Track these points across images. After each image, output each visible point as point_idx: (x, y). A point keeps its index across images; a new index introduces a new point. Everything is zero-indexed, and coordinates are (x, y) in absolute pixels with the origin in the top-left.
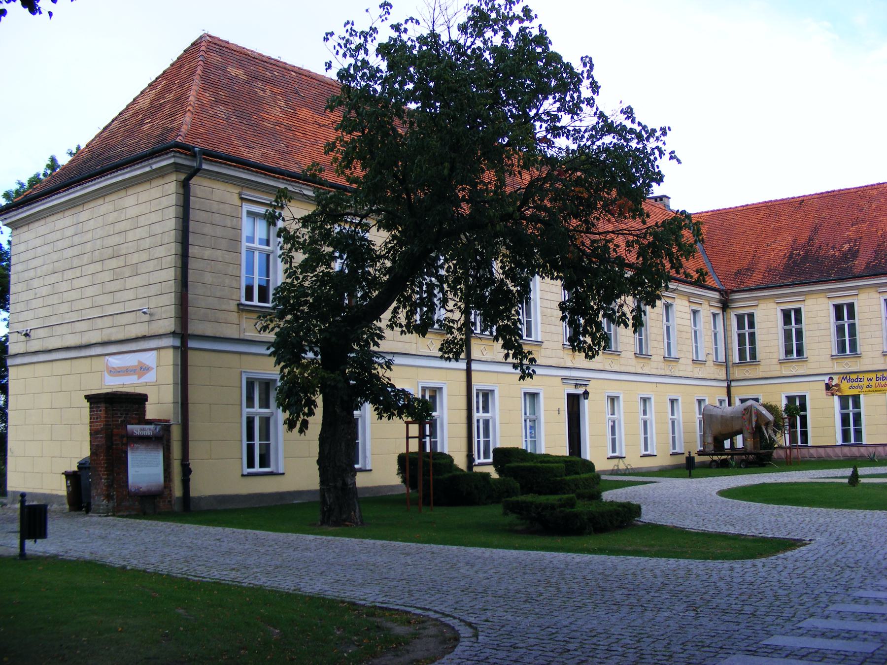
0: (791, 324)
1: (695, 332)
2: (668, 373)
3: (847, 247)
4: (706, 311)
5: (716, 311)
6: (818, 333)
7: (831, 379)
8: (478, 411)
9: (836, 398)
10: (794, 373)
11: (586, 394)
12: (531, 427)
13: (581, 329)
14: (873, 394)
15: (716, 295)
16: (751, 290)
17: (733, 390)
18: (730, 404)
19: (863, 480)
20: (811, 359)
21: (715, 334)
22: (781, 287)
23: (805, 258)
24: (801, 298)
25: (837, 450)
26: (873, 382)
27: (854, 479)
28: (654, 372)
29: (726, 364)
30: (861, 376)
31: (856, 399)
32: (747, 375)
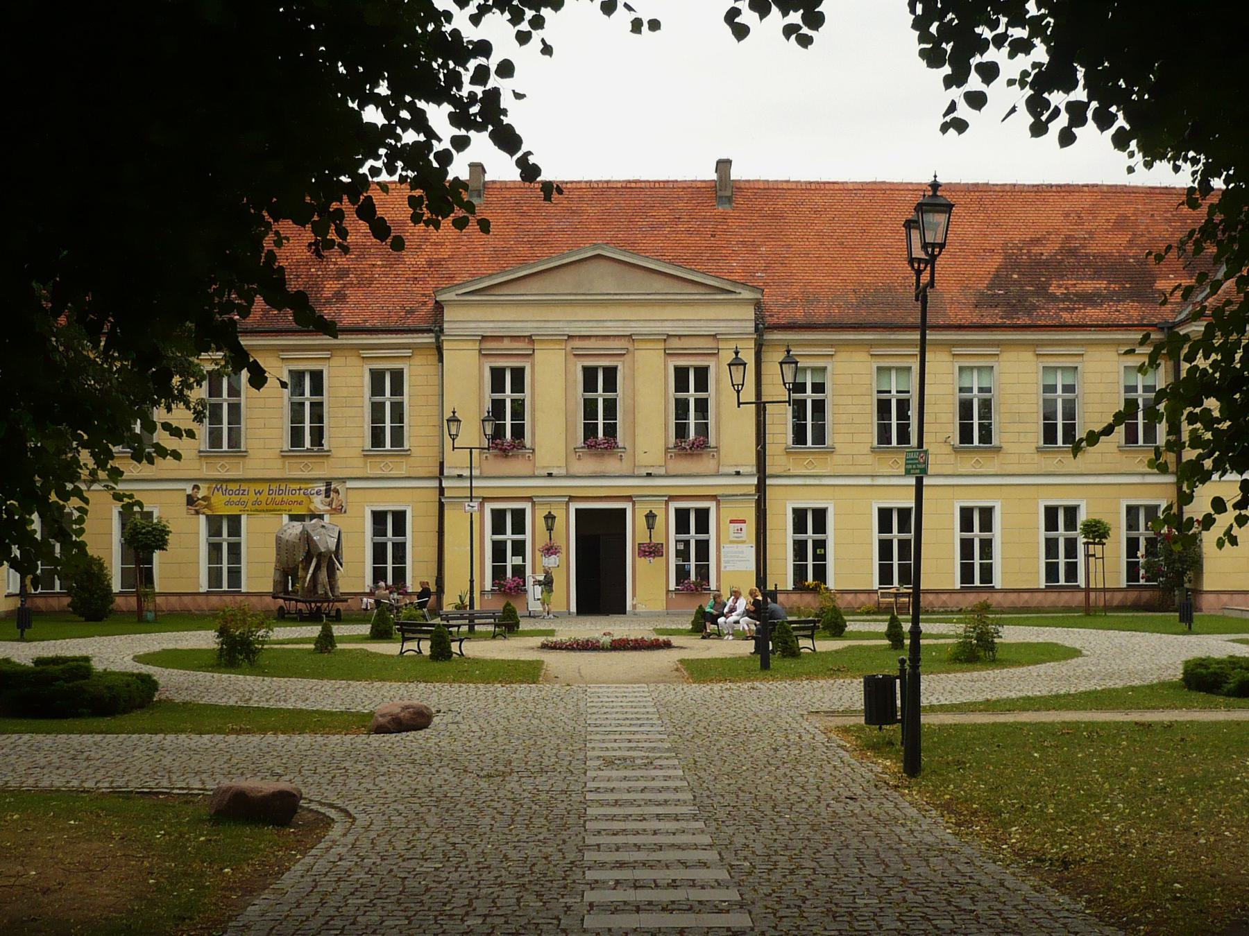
7: (196, 487)
9: (202, 518)
14: (262, 515)
16: (960, 327)
18: (744, 522)
19: (339, 646)
24: (408, 353)
25: (1040, 596)
26: (263, 498)
30: (244, 486)
31: (235, 522)
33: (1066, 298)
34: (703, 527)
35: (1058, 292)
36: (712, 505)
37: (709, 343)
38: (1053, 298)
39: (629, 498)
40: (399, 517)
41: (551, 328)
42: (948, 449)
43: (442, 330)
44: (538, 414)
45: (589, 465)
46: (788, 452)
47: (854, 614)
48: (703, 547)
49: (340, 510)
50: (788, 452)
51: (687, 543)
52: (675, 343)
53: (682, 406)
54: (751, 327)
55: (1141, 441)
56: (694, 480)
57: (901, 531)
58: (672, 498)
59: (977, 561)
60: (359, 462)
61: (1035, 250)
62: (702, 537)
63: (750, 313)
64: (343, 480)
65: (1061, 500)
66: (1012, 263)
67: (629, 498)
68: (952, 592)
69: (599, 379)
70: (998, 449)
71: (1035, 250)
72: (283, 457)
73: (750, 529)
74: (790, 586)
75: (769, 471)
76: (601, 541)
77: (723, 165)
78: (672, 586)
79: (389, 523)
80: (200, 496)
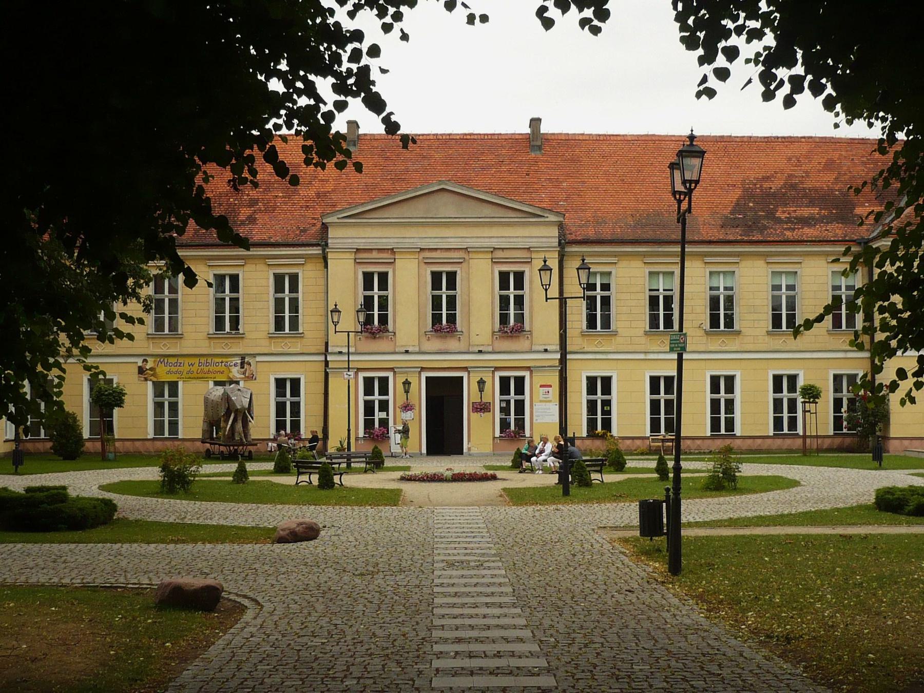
9: (150, 384)
14: (194, 381)
16: (710, 242)
19: (251, 478)
24: (302, 261)
26: (194, 369)
27: (241, 475)
30: (181, 360)
31: (174, 387)
32: (286, 350)
33: (789, 220)
34: (520, 390)
35: (783, 216)
36: (527, 374)
37: (525, 254)
38: (779, 221)
39: (465, 369)
40: (295, 383)
41: (408, 243)
42: (701, 333)
43: (327, 245)
44: (398, 307)
46: (583, 334)
47: (632, 454)
48: (520, 405)
49: (252, 377)
50: (583, 334)
51: (508, 402)
52: (499, 254)
53: (504, 301)
54: (555, 242)
55: (844, 327)
56: (513, 356)
57: (666, 393)
58: (497, 369)
59: (723, 416)
60: (266, 342)
61: (766, 185)
62: (519, 397)
63: (555, 232)
64: (254, 355)
65: (785, 370)
66: (748, 194)
67: (465, 369)
68: (704, 438)
69: (443, 280)
70: (739, 333)
71: (766, 185)
72: (210, 338)
73: (555, 391)
74: (585, 434)
75: (569, 349)
76: (444, 400)
78: (497, 434)
79: (288, 387)
80: (148, 367)
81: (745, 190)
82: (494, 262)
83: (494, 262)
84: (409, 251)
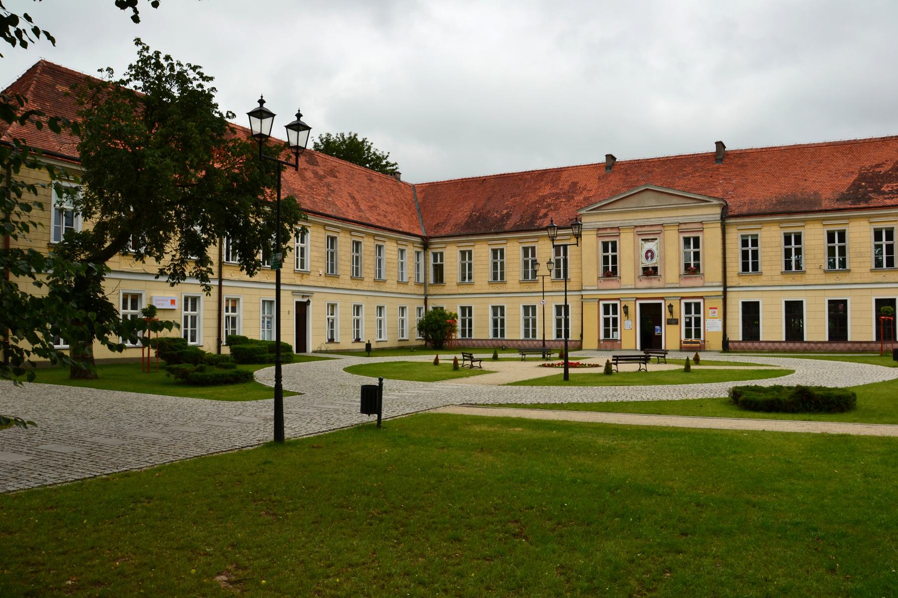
0: (887, 245)
1: (402, 263)
2: (377, 289)
3: (505, 212)
4: (410, 251)
5: (419, 250)
6: (481, 267)
8: (227, 311)
10: (465, 291)
11: (309, 301)
12: (268, 322)
13: (33, 270)
15: (419, 240)
16: (826, 211)
17: (428, 302)
20: (476, 283)
21: (418, 265)
22: (460, 236)
23: (478, 218)
28: (366, 288)
29: (425, 284)
32: (437, 292)
33: (891, 192)
34: (698, 311)
35: (886, 190)
36: (701, 301)
37: (699, 226)
38: (884, 193)
39: (662, 298)
40: (534, 307)
41: (627, 223)
42: (822, 272)
45: (645, 283)
46: (739, 275)
48: (698, 321)
50: (739, 275)
51: (690, 318)
52: (683, 227)
53: (606, 259)
54: (718, 217)
56: (693, 288)
58: (683, 298)
59: (499, 328)
61: (877, 170)
62: (697, 315)
63: (718, 211)
66: (862, 177)
67: (662, 298)
68: (872, 342)
70: (849, 271)
71: (877, 170)
73: (719, 312)
75: (728, 284)
76: (651, 315)
77: (720, 145)
81: (861, 174)
82: (680, 232)
83: (680, 232)
84: (628, 227)
